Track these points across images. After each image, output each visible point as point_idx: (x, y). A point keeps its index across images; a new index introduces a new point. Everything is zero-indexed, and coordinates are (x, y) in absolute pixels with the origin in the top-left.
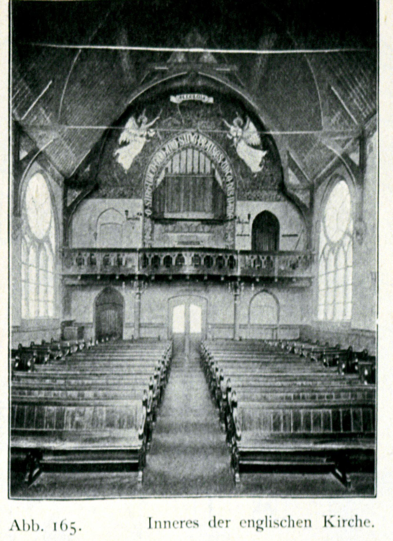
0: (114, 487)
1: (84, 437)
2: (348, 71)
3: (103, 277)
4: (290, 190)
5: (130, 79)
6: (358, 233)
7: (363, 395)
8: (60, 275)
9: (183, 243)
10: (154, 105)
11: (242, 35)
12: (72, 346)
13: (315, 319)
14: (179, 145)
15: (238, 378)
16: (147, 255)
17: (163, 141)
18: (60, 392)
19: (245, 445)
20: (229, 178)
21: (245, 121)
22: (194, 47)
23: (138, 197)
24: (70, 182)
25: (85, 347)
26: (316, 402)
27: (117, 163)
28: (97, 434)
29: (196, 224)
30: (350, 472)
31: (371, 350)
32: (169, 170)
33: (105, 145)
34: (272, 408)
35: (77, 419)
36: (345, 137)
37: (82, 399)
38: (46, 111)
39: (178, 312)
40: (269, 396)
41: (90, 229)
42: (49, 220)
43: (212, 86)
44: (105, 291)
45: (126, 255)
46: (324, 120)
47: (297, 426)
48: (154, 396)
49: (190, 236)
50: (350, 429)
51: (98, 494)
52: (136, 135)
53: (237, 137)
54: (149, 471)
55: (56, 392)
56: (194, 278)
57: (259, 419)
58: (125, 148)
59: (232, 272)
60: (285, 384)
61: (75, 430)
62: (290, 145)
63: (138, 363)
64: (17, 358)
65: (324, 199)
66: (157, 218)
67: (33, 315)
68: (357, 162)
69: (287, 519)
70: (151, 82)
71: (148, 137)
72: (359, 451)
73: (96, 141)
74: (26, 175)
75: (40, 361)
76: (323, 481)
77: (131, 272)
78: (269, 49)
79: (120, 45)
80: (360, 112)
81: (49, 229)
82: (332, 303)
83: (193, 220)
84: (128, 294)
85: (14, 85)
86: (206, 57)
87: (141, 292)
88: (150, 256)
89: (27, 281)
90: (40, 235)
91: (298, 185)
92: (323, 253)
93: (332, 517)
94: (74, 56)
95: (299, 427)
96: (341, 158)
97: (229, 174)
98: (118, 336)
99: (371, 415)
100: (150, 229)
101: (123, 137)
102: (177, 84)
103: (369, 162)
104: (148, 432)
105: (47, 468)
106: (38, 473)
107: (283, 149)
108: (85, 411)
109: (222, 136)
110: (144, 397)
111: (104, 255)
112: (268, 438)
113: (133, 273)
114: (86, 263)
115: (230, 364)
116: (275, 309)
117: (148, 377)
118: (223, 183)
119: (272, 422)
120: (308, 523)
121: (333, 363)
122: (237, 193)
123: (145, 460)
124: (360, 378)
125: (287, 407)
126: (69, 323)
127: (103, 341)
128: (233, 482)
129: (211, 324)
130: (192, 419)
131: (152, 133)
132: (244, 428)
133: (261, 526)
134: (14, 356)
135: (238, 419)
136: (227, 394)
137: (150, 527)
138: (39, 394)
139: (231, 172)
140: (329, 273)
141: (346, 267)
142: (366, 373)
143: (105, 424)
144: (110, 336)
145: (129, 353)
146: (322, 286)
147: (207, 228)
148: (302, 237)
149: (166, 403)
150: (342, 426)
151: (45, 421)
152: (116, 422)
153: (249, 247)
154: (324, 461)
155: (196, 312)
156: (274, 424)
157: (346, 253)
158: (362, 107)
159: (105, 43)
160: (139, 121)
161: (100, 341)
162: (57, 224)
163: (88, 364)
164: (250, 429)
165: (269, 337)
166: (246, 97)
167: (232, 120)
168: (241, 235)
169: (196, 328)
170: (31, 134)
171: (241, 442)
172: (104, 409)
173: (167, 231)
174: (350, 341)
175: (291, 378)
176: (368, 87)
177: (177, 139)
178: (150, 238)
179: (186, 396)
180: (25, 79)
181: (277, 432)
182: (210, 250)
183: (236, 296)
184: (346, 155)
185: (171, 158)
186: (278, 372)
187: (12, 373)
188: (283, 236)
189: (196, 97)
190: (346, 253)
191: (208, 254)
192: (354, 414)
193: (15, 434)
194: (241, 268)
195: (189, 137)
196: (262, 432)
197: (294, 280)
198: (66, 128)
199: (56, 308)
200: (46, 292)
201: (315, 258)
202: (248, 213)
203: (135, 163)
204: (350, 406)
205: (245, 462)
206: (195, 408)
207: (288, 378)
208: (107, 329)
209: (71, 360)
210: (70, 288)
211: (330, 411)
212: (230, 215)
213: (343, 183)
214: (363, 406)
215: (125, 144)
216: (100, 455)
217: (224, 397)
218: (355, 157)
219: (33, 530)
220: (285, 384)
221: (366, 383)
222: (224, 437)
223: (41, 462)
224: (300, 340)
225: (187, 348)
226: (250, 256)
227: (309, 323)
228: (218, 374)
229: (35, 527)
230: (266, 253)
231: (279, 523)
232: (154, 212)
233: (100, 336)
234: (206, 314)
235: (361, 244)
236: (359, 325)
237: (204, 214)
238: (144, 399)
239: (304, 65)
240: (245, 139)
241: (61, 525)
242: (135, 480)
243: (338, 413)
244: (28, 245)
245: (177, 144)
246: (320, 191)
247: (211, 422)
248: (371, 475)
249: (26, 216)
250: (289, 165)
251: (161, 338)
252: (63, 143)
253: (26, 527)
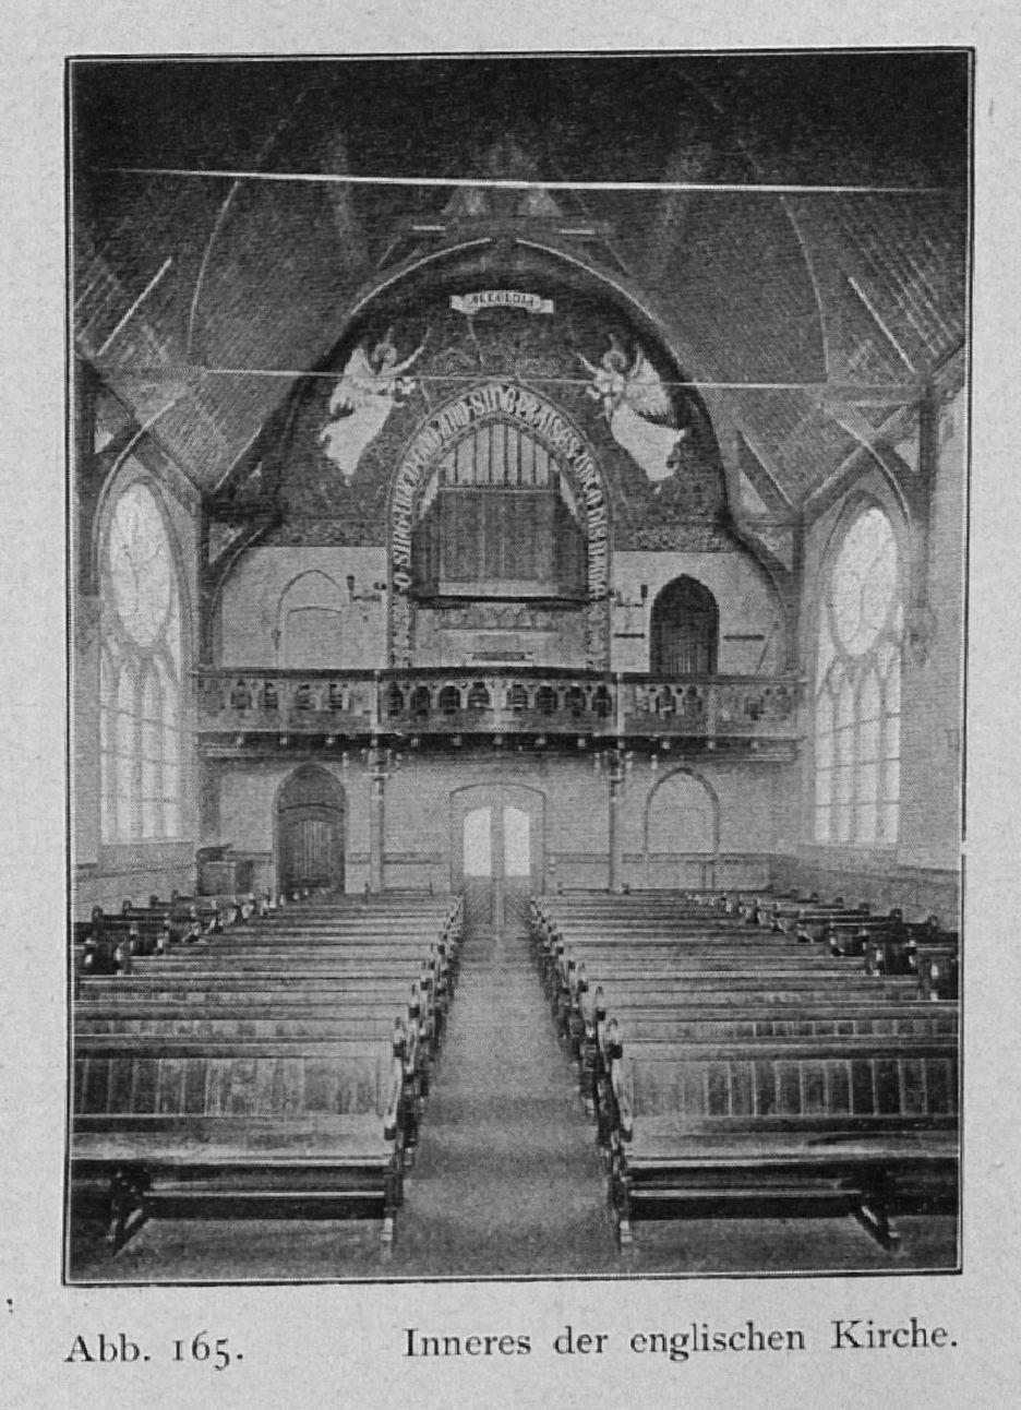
0: (325, 1256)
1: (256, 1133)
2: (894, 243)
3: (296, 741)
4: (744, 528)
5: (354, 256)
6: (915, 637)
7: (929, 1028)
8: (194, 734)
9: (487, 656)
10: (412, 317)
11: (624, 147)
12: (223, 908)
13: (807, 842)
14: (472, 413)
15: (621, 986)
16: (401, 683)
17: (434, 404)
18: (197, 1023)
19: (643, 1151)
20: (594, 497)
21: (632, 360)
22: (506, 177)
23: (375, 543)
24: (217, 505)
25: (254, 912)
26: (811, 1042)
27: (326, 459)
28: (287, 1128)
29: (516, 608)
30: (894, 1214)
31: (947, 918)
32: (451, 477)
33: (296, 416)
34: (706, 1058)
35: (236, 1089)
36: (885, 403)
37: (249, 1041)
38: (158, 332)
39: (477, 823)
40: (699, 1029)
41: (265, 621)
42: (166, 602)
43: (552, 271)
44: (301, 775)
45: (352, 687)
46: (830, 360)
47: (767, 1101)
48: (423, 1032)
49: (504, 639)
50: (896, 1109)
51: (284, 1272)
52: (368, 392)
53: (613, 394)
54: (411, 1216)
55: (185, 1023)
56: (518, 744)
57: (675, 1088)
58: (343, 424)
59: (603, 726)
60: (735, 997)
61: (230, 1115)
62: (743, 415)
63: (380, 952)
64: (88, 942)
65: (830, 551)
66: (424, 597)
67: (127, 836)
68: (913, 465)
69: (746, 1331)
70: (406, 261)
71: (398, 396)
72: (919, 1164)
73: (276, 405)
74: (108, 491)
75: (145, 949)
76: (833, 1238)
77: (362, 730)
78: (690, 180)
79: (332, 172)
80: (923, 344)
81: (168, 621)
82: (847, 804)
83: (510, 600)
84: (355, 780)
85: (80, 273)
86: (534, 201)
87: (386, 775)
88: (409, 689)
89: (114, 752)
90: (145, 637)
91: (763, 516)
92: (827, 681)
93: (854, 1323)
94: (224, 195)
95: (774, 1107)
96: (872, 450)
97: (594, 486)
98: (334, 887)
99: (949, 1076)
100: (408, 621)
101: (338, 398)
102: (466, 268)
103: (944, 461)
104: (408, 1123)
105: (163, 1208)
106: (140, 1222)
107: (725, 426)
108: (255, 1069)
109: (576, 391)
110: (398, 1036)
111: (297, 684)
112: (696, 1133)
113: (367, 730)
114: (255, 704)
115: (602, 952)
116: (710, 813)
117: (407, 986)
118: (580, 508)
119: (707, 1095)
120: (796, 1340)
121: (854, 949)
122: (613, 533)
123: (401, 1192)
124: (921, 987)
125: (741, 1057)
126: (215, 854)
127: (296, 897)
128: (615, 1244)
129: (555, 854)
130: (515, 1090)
131: (408, 387)
132: (639, 1110)
134: (80, 939)
135: (624, 1088)
136: (595, 1025)
137: (411, 1353)
138: (143, 1028)
139: (597, 479)
140: (841, 730)
141: (886, 716)
142: (935, 972)
143: (302, 1103)
144: (314, 885)
145: (363, 925)
146: (825, 762)
147: (543, 618)
148: (775, 642)
149: (448, 1049)
150: (875, 1102)
151: (158, 1097)
152: (332, 1099)
153: (644, 666)
154: (835, 1188)
155: (518, 822)
156: (712, 1096)
157: (883, 684)
158: (927, 330)
159: (296, 169)
160: (376, 358)
161: (290, 898)
162: (185, 606)
163: (263, 953)
164: (656, 1113)
165: (694, 884)
166: (633, 298)
167: (601, 356)
168: (625, 636)
169: (519, 864)
170: (119, 390)
171: (632, 1145)
172: (301, 1064)
173: (446, 626)
174: (896, 895)
175: (751, 984)
176: (944, 281)
177: (468, 402)
178: (407, 642)
179: (498, 1031)
180: (108, 257)
181: (720, 1118)
182: (552, 673)
183: (614, 783)
184: (885, 447)
185: (455, 445)
186: (720, 969)
187: (77, 979)
188: (727, 638)
189: (512, 298)
190: (883, 684)
191: (545, 683)
192: (907, 1071)
193: (82, 1129)
194: (626, 715)
195: (497, 394)
196: (684, 1116)
197: (755, 745)
198: (205, 373)
199: (185, 815)
200: (159, 776)
201: (807, 692)
202: (641, 582)
203: (368, 460)
204: (897, 1052)
205: (645, 1194)
206: (520, 1062)
207: (744, 984)
208: (304, 869)
209: (222, 943)
210: (218, 762)
211: (848, 1063)
212: (595, 585)
213: (876, 513)
214: (929, 1053)
215: (345, 412)
216: (292, 1180)
217: (590, 1033)
218: (909, 452)
219: (124, 1358)
220: (735, 997)
221: (934, 998)
222: (592, 1132)
223: (146, 1194)
224: (769, 891)
225: (499, 912)
226: (648, 687)
227: (791, 851)
228: (574, 977)
229: (130, 1352)
230: (684, 679)
231: (727, 1341)
232: (417, 583)
233: (289, 885)
234: (542, 830)
235: (922, 661)
236: (923, 858)
237: (533, 584)
238: (397, 1042)
239: (782, 223)
240: (632, 401)
241: (195, 1347)
242: (376, 1238)
243: (867, 1069)
244: (116, 664)
245: (467, 413)
246: (819, 530)
247: (559, 1097)
248: (949, 1218)
249: (111, 592)
250: (742, 464)
251: (435, 891)
252: (193, 413)
253: (109, 1352)
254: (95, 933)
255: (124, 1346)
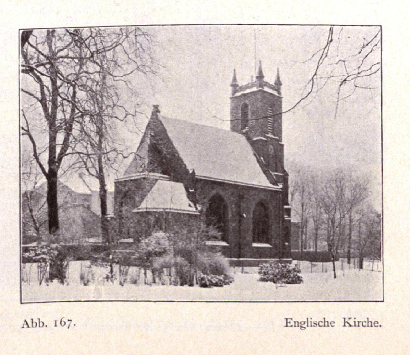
93: (350, 318)
133: (304, 326)
219: (39, 326)
229: (41, 324)
231: (317, 323)
241: (61, 322)
253: (34, 325)
254: (173, 171)
255: (39, 322)
